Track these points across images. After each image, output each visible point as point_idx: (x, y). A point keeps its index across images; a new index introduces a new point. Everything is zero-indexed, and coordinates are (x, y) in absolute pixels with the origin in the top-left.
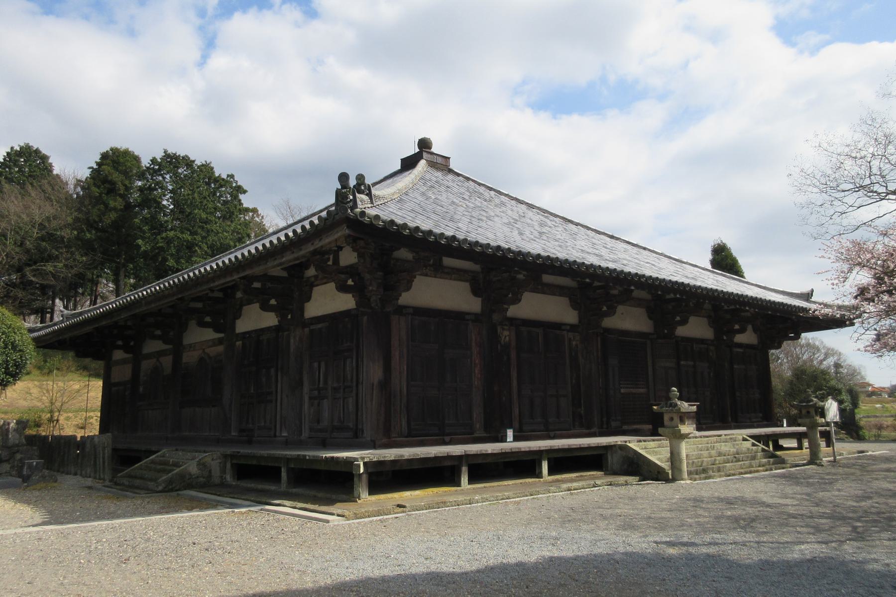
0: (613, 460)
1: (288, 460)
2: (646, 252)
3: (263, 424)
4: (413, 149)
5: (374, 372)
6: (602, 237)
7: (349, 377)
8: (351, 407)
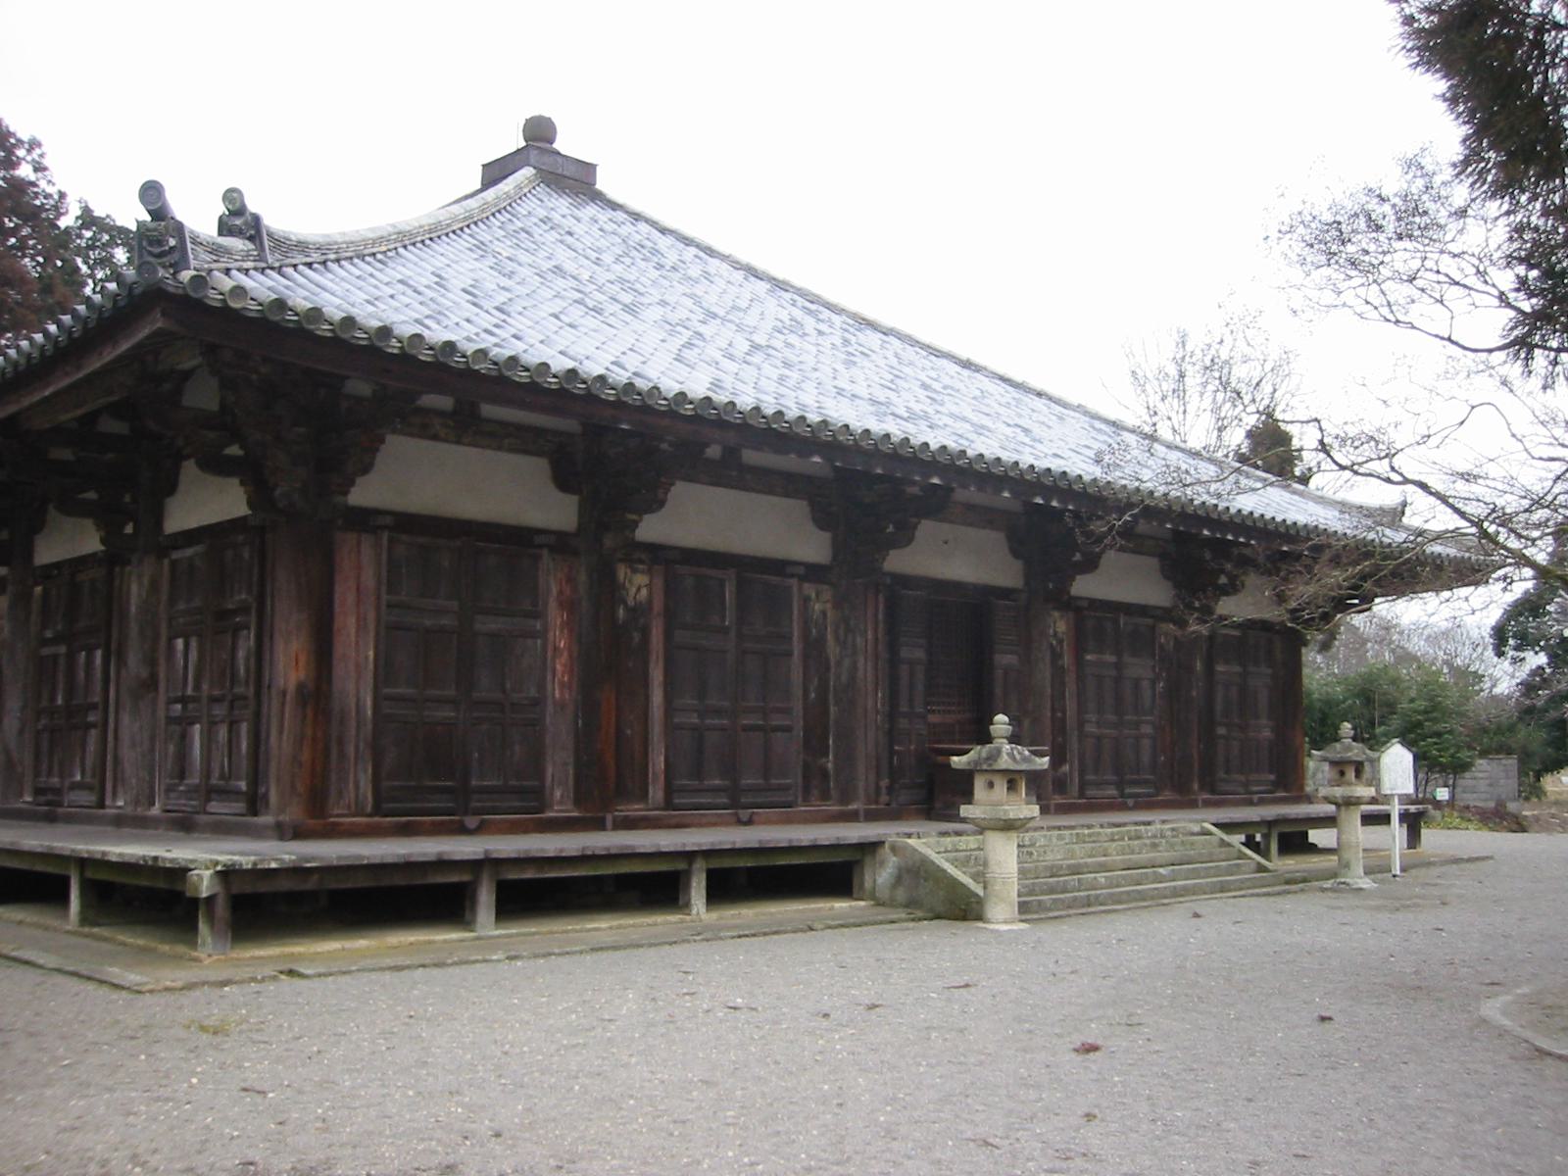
0: (881, 875)
1: (83, 863)
2: (1039, 404)
3: (78, 778)
5: (289, 665)
6: (944, 362)
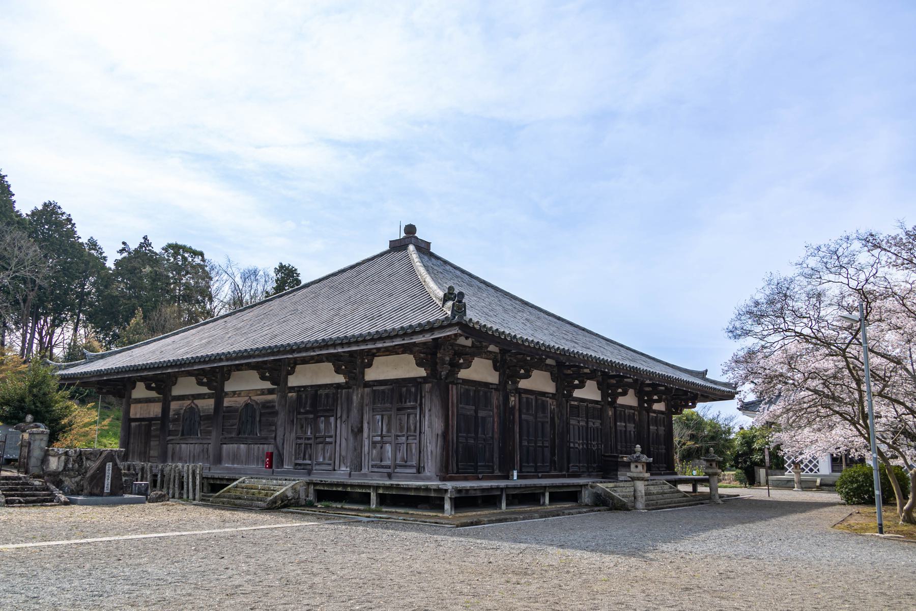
0: (586, 497)
4: (398, 234)
7: (412, 428)
8: (414, 450)
